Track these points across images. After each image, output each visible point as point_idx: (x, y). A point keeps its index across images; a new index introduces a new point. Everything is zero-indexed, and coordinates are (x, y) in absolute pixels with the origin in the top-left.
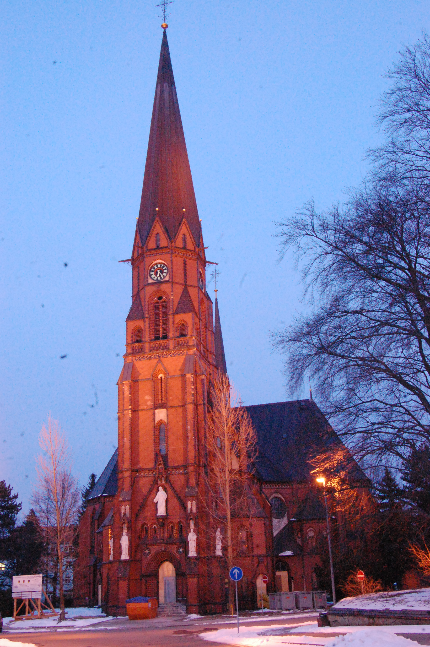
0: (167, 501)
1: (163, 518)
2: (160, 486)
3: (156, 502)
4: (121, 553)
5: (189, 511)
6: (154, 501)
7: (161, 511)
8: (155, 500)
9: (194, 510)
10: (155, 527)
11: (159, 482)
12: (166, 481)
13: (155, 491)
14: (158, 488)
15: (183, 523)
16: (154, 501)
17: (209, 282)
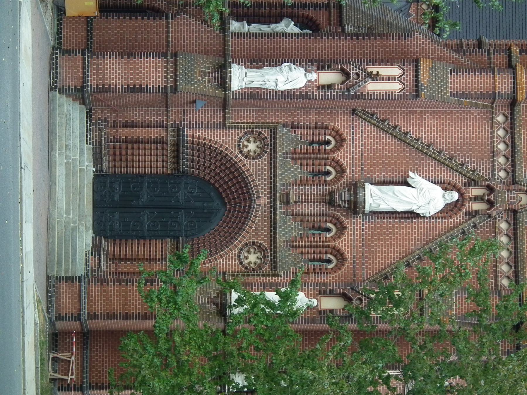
0: (411, 215)
1: (355, 207)
2: (461, 195)
3: (410, 181)
5: (373, 69)
8: (414, 178)
9: (372, 86)
10: (328, 173)
14: (453, 187)
15: (338, 267)
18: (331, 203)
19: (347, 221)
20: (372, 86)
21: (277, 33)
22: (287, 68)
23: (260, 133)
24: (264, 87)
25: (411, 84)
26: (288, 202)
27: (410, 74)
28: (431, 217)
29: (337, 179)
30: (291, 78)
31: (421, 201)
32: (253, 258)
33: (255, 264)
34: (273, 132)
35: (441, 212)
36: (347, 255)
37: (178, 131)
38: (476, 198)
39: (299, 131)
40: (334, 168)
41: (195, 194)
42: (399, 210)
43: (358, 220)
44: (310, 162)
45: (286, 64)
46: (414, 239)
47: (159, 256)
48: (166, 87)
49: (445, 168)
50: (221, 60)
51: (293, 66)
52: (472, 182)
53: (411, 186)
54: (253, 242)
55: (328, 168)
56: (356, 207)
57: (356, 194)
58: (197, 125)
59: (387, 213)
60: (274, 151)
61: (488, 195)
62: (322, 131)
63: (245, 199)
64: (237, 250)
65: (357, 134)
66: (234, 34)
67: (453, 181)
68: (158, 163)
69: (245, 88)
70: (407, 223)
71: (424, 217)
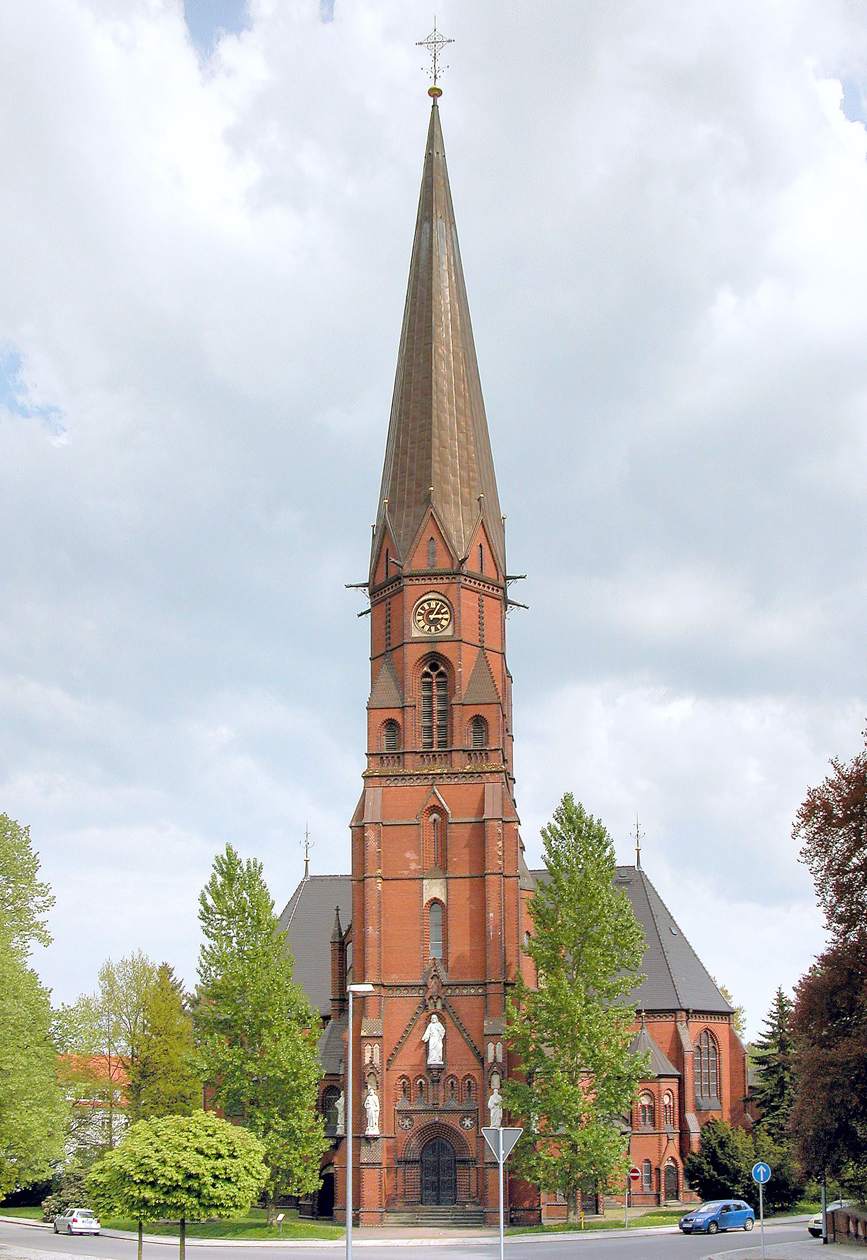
0: (444, 1040)
1: (440, 1069)
2: (433, 1013)
5: (367, 1061)
7: (435, 1057)
8: (425, 1038)
9: (377, 1061)
20: (377, 1061)
27: (370, 1041)
30: (373, 1103)
46: (458, 1040)
50: (363, 1140)
65: (399, 1068)
68: (414, 1173)
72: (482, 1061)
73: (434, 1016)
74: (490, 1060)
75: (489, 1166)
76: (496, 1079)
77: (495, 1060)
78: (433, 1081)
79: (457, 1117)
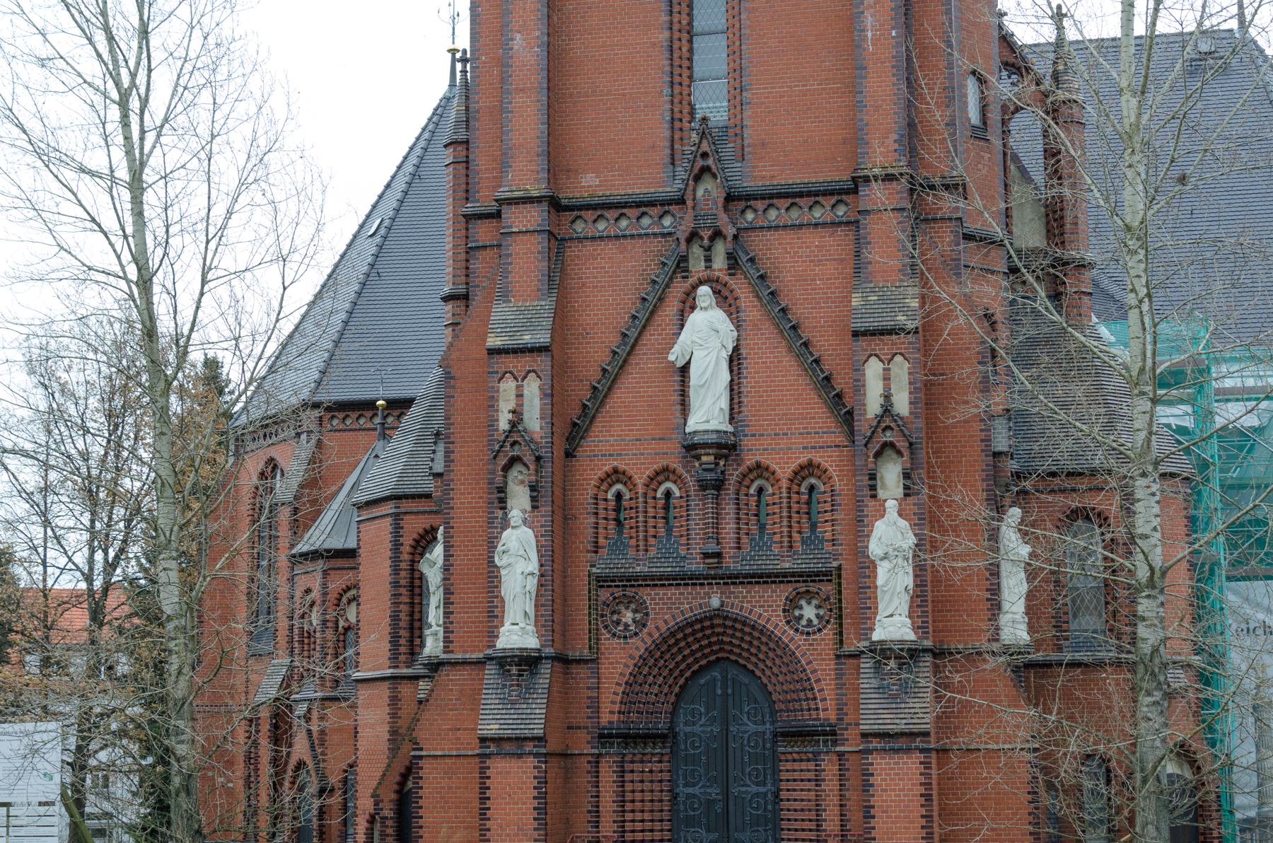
0: (735, 360)
1: (726, 448)
2: (701, 283)
3: (680, 364)
4: (493, 614)
6: (671, 358)
7: (708, 413)
8: (676, 355)
10: (668, 494)
11: (697, 265)
12: (733, 262)
13: (670, 309)
16: (671, 358)
17: (715, 374)
18: (719, 485)
19: (749, 460)
21: (444, 579)
22: (505, 557)
23: (604, 603)
24: (534, 595)
25: (524, 362)
26: (718, 555)
28: (738, 327)
29: (678, 480)
31: (715, 343)
32: (809, 612)
33: (818, 607)
34: (602, 581)
35: (730, 315)
36: (803, 459)
37: (604, 737)
38: (708, 260)
39: (601, 541)
40: (660, 484)
41: (703, 710)
42: (729, 379)
43: (746, 443)
44: (651, 522)
45: (496, 559)
47: (811, 766)
48: (536, 755)
49: (661, 303)
50: (491, 670)
51: (500, 548)
52: (682, 264)
53: (689, 363)
54: (784, 611)
55: (659, 495)
56: (725, 446)
57: (705, 445)
58: (595, 706)
59: (732, 399)
60: (632, 580)
61: (702, 238)
62: (602, 505)
63: (712, 626)
64: (798, 637)
66: (446, 650)
67: (680, 295)
69: (536, 626)
70: (749, 367)
71: (738, 340)
72: (848, 419)
73: (704, 290)
74: (873, 405)
75: (875, 744)
76: (891, 474)
77: (887, 409)
78: (703, 486)
79: (778, 595)
